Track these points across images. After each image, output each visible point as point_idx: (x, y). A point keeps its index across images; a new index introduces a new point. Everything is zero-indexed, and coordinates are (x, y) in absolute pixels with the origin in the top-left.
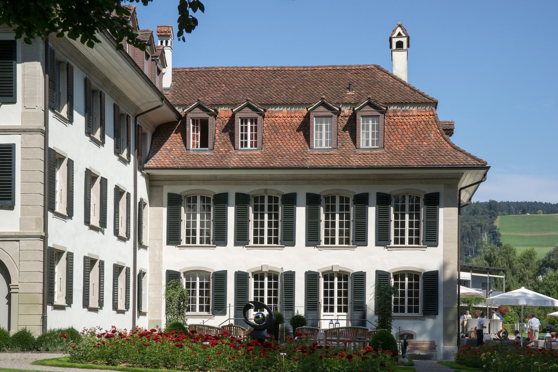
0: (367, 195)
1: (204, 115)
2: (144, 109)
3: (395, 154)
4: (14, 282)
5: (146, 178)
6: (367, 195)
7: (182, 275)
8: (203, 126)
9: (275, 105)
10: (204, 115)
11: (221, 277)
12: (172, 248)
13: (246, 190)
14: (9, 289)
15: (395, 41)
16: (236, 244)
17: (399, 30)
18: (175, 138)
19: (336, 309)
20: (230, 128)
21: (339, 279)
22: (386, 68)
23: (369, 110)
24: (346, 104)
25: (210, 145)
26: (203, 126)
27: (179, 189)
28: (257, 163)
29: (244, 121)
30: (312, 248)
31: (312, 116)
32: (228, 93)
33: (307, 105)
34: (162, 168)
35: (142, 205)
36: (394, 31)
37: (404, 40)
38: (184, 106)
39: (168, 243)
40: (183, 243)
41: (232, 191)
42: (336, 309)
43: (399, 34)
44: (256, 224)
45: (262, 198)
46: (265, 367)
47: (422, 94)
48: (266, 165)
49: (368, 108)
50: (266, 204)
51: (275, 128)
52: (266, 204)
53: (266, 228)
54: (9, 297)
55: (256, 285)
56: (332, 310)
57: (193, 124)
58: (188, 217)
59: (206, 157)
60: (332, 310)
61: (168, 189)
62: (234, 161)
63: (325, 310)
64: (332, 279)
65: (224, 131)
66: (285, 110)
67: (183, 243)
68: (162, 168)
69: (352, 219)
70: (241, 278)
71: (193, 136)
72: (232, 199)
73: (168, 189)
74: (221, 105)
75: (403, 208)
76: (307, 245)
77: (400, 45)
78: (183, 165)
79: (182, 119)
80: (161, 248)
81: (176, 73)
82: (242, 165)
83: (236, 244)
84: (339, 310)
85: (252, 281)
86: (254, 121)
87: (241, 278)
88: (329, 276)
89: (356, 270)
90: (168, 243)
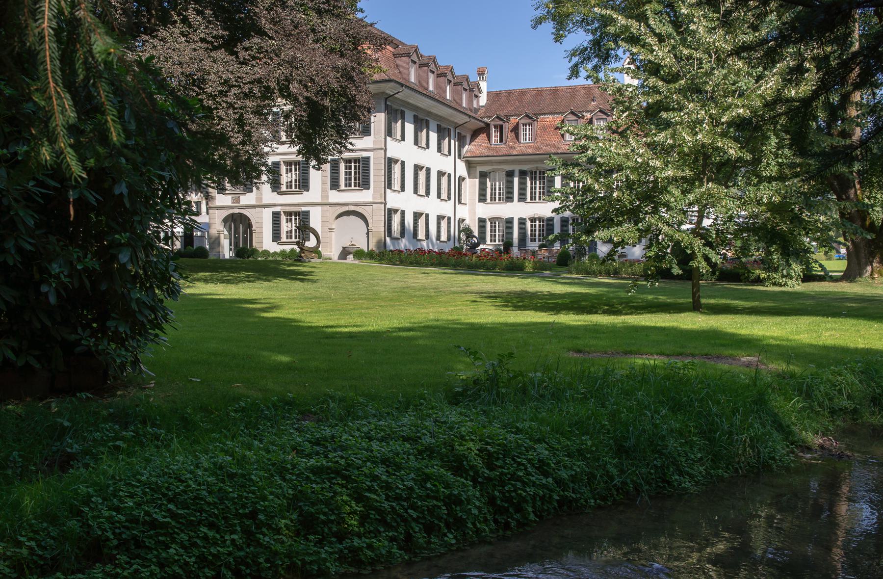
0: (514, 171)
1: (500, 123)
2: (461, 123)
4: (370, 226)
6: (514, 171)
7: (487, 220)
8: (501, 129)
9: (545, 114)
10: (500, 123)
11: (509, 221)
12: (482, 204)
13: (525, 167)
14: (368, 230)
16: (519, 201)
18: (483, 137)
19: (537, 240)
20: (515, 130)
21: (540, 222)
23: (572, 117)
24: (588, 112)
25: (504, 141)
26: (501, 129)
27: (485, 169)
28: (530, 151)
29: (524, 125)
31: (594, 119)
32: (518, 107)
33: (562, 113)
34: (474, 157)
35: (462, 179)
38: (489, 117)
39: (480, 201)
40: (528, 200)
41: (517, 168)
42: (537, 240)
44: (531, 188)
45: (535, 172)
48: (535, 152)
49: (599, 114)
50: (538, 176)
51: (544, 128)
52: (538, 176)
54: (368, 234)
55: (491, 226)
56: (535, 240)
57: (495, 128)
58: (532, 184)
59: (500, 149)
60: (535, 240)
61: (479, 169)
62: (517, 151)
63: (531, 241)
64: (535, 222)
65: (511, 131)
66: (551, 117)
67: (528, 200)
68: (474, 157)
70: (522, 222)
71: (495, 135)
72: (517, 173)
73: (479, 169)
74: (512, 116)
75: (535, 179)
78: (486, 154)
79: (488, 125)
81: (490, 95)
82: (521, 152)
83: (519, 201)
85: (488, 224)
86: (530, 124)
87: (522, 222)
88: (493, 220)
89: (508, 217)
90: (480, 201)
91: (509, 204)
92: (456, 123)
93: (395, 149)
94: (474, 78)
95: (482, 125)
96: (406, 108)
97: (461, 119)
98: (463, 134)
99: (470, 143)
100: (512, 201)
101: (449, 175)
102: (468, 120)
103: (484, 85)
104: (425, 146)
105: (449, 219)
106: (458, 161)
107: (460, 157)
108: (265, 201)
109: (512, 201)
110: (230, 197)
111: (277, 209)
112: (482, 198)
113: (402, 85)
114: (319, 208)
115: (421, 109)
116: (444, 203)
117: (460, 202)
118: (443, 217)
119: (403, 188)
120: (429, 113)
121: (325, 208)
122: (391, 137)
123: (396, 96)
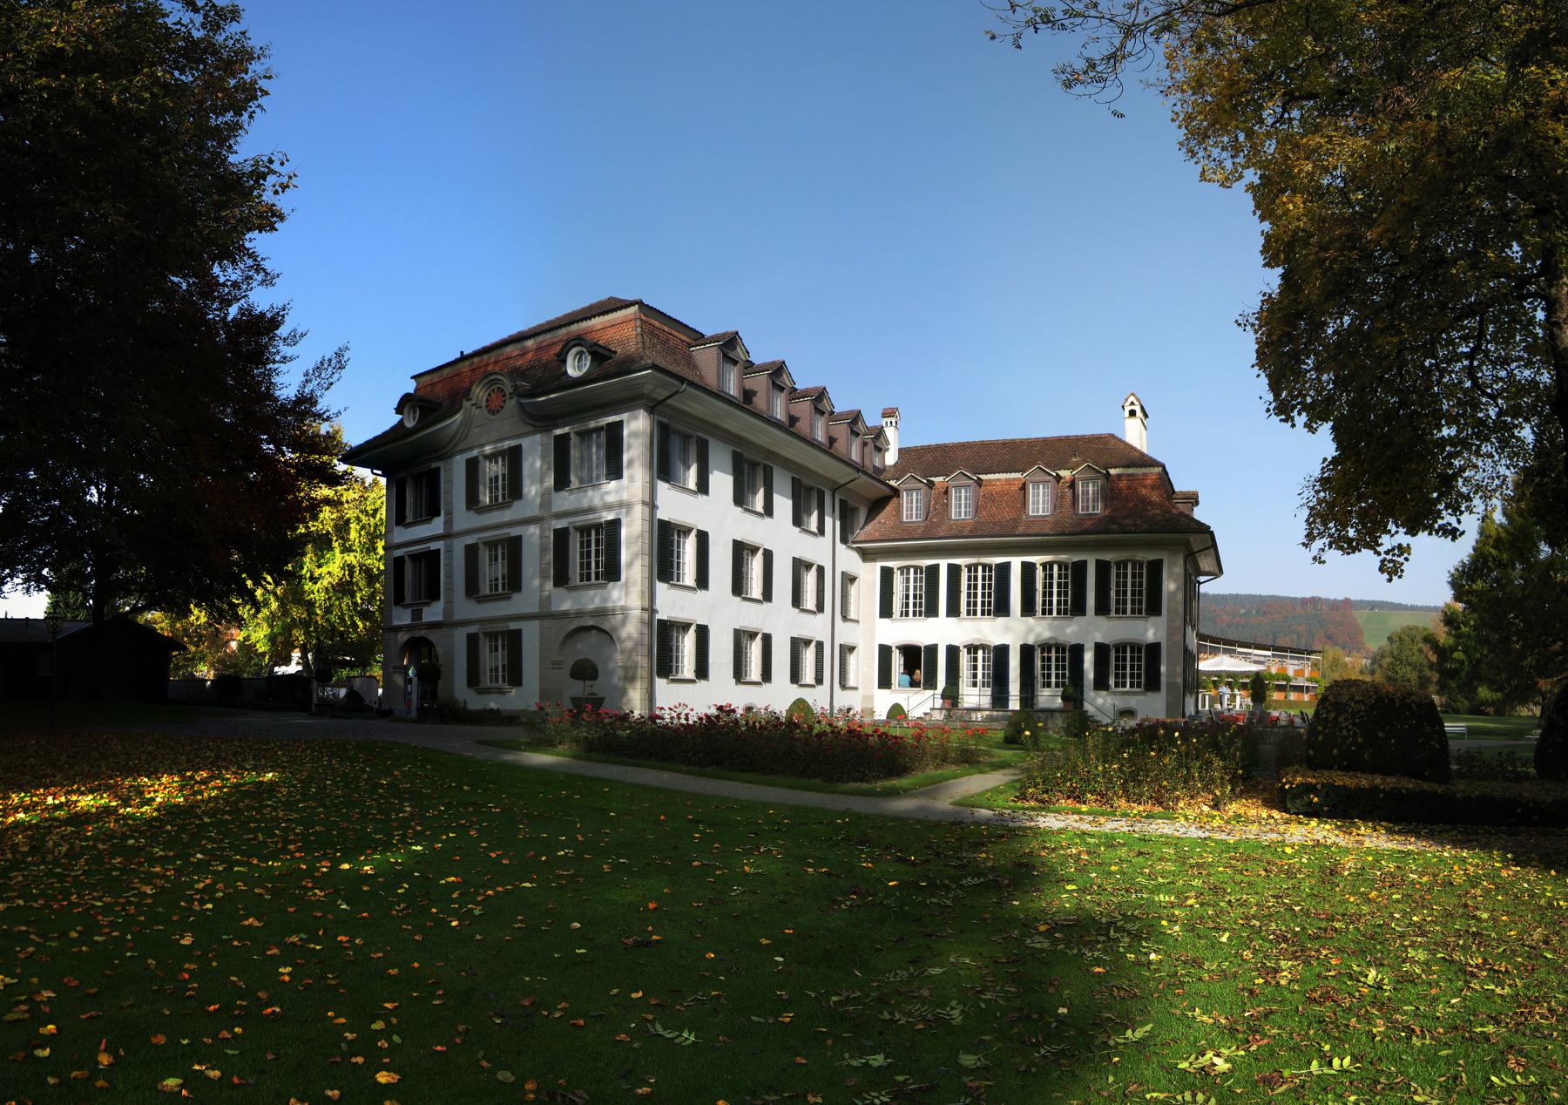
2: (843, 482)
3: (549, 469)
5: (858, 553)
12: (886, 621)
15: (1128, 409)
17: (1132, 399)
21: (1057, 652)
22: (1120, 437)
30: (953, 619)
36: (1126, 400)
37: (1137, 408)
43: (1132, 403)
46: (24, 928)
47: (701, 377)
53: (979, 599)
64: (1049, 652)
69: (1144, 586)
70: (953, 652)
76: (947, 616)
77: (1133, 413)
80: (874, 622)
84: (1057, 685)
87: (953, 652)
91: (931, 620)
92: (834, 482)
93: (675, 504)
94: (871, 419)
95: (888, 491)
96: (713, 435)
97: (841, 474)
98: (851, 503)
99: (867, 521)
100: (937, 616)
101: (821, 570)
102: (856, 475)
103: (890, 433)
104: (815, 530)
105: (820, 645)
106: (840, 547)
107: (844, 540)
108: (459, 615)
109: (937, 616)
110: (409, 611)
111: (474, 629)
112: (886, 611)
113: (682, 380)
114: (536, 624)
115: (749, 442)
116: (811, 616)
117: (845, 618)
118: (808, 643)
119: (767, 595)
120: (771, 454)
121: (549, 623)
122: (667, 480)
123: (670, 401)
